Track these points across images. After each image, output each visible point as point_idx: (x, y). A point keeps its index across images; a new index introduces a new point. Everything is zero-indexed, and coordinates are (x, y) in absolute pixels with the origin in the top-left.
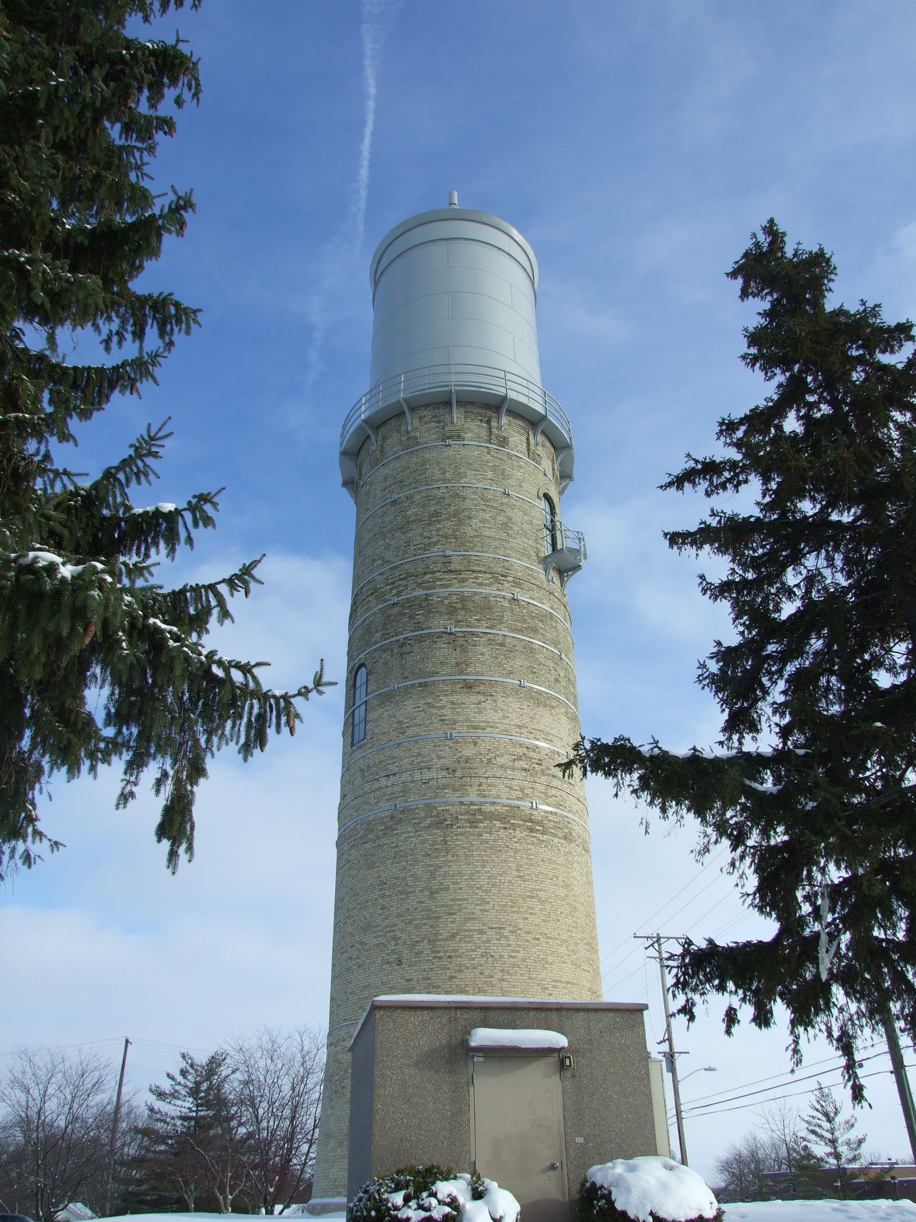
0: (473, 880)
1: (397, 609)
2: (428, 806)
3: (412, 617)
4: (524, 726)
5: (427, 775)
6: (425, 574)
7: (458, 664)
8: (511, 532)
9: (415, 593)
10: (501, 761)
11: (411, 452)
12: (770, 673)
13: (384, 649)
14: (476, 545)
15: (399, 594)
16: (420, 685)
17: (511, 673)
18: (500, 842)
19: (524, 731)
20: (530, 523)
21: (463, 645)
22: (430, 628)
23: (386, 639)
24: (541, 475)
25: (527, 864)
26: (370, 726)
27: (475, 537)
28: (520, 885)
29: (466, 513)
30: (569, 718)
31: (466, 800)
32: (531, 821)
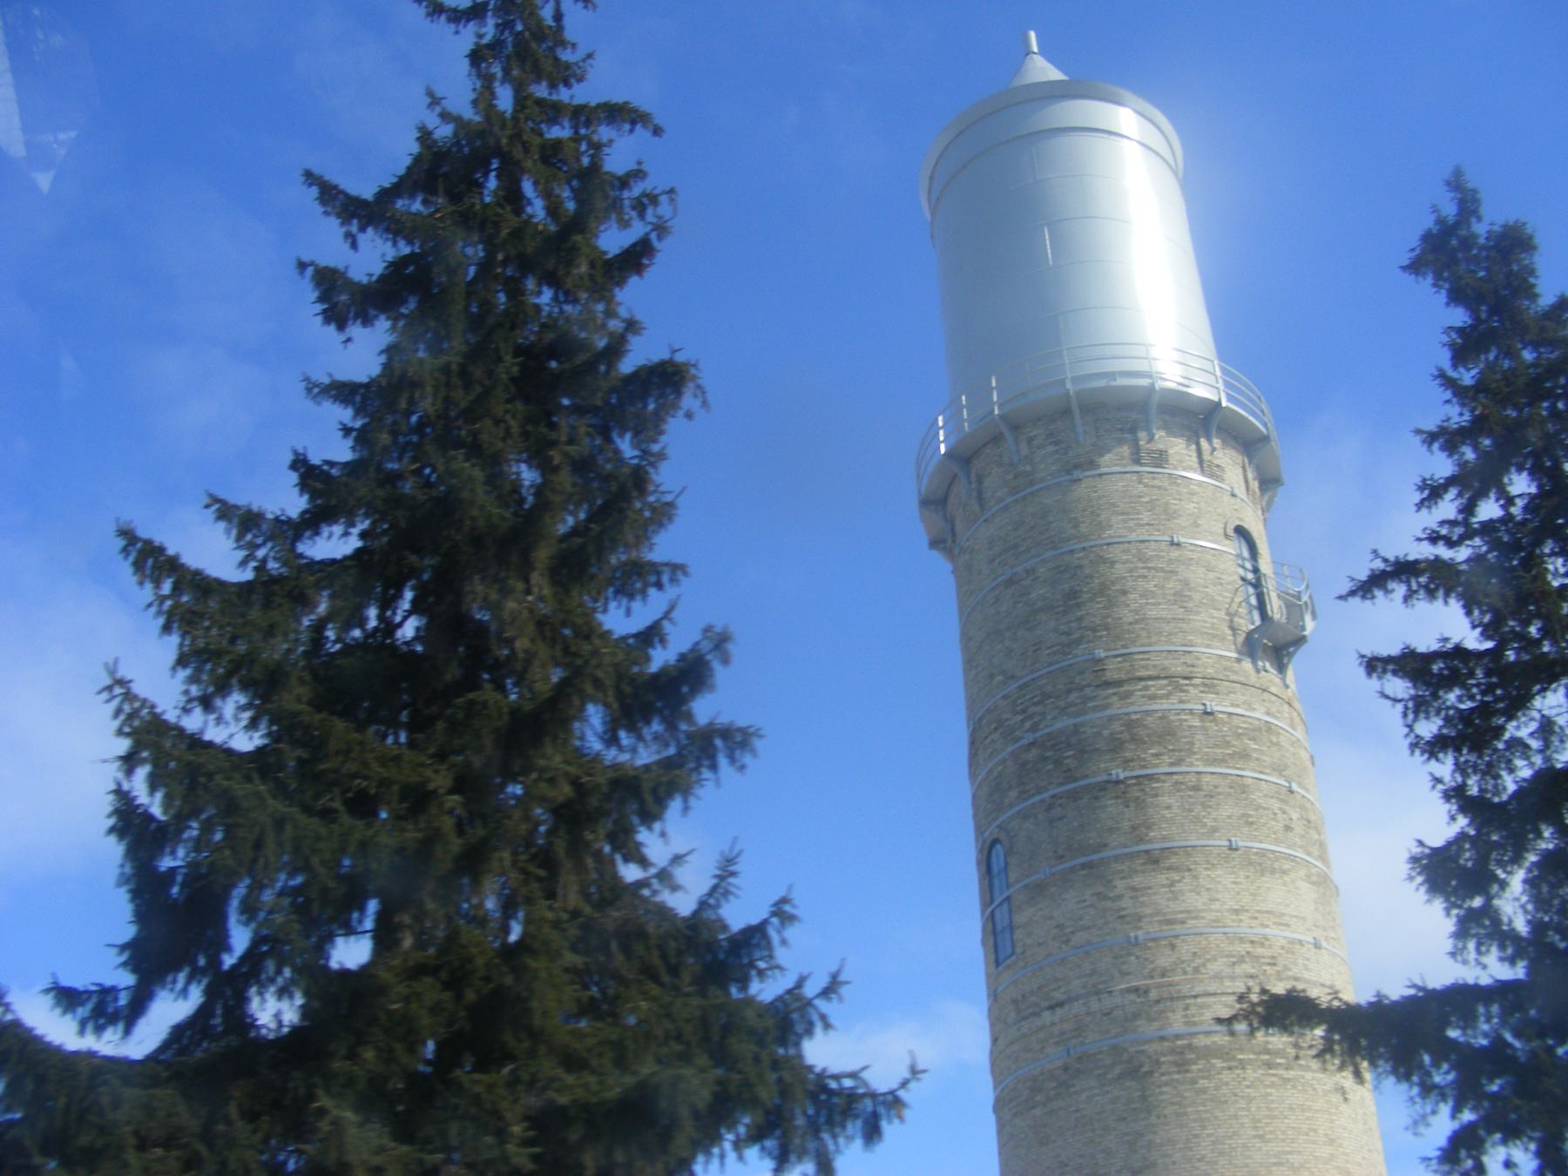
0: (1191, 1149)
1: (1034, 752)
2: (1114, 1048)
3: (1057, 762)
4: (1242, 910)
5: (1108, 1002)
6: (1069, 692)
7: (1134, 828)
8: (1190, 605)
9: (1059, 725)
10: (1213, 967)
11: (1024, 498)
12: (1500, 863)
13: (1024, 816)
14: (1138, 636)
15: (1034, 729)
16: (1083, 866)
17: (1215, 830)
18: (1224, 1090)
19: (1244, 916)
20: (1218, 582)
21: (1137, 798)
22: (1086, 776)
23: (1025, 800)
24: (1226, 498)
25: (1267, 1117)
26: (1018, 934)
27: (1137, 622)
28: (1260, 1149)
29: (1118, 587)
30: (1314, 883)
31: (1170, 1031)
32: (1268, 1052)
